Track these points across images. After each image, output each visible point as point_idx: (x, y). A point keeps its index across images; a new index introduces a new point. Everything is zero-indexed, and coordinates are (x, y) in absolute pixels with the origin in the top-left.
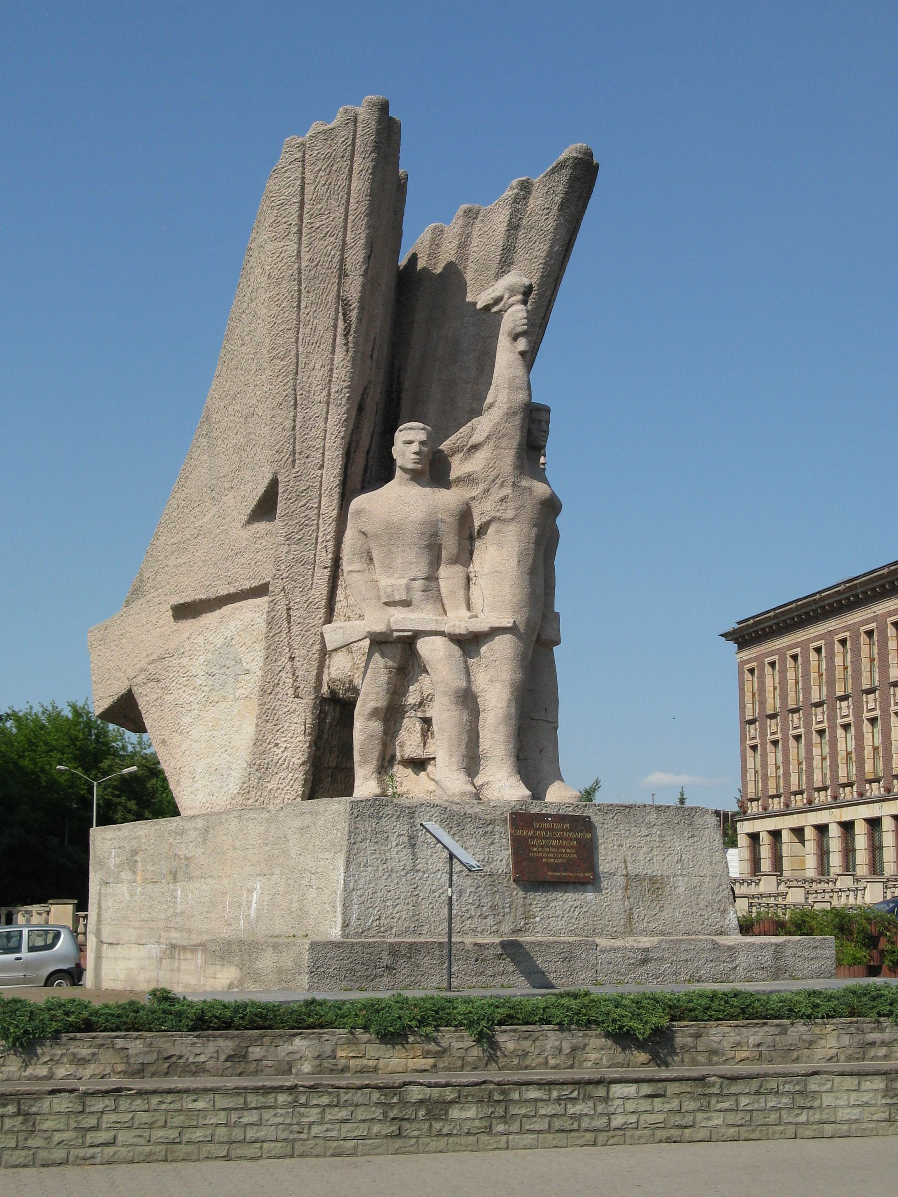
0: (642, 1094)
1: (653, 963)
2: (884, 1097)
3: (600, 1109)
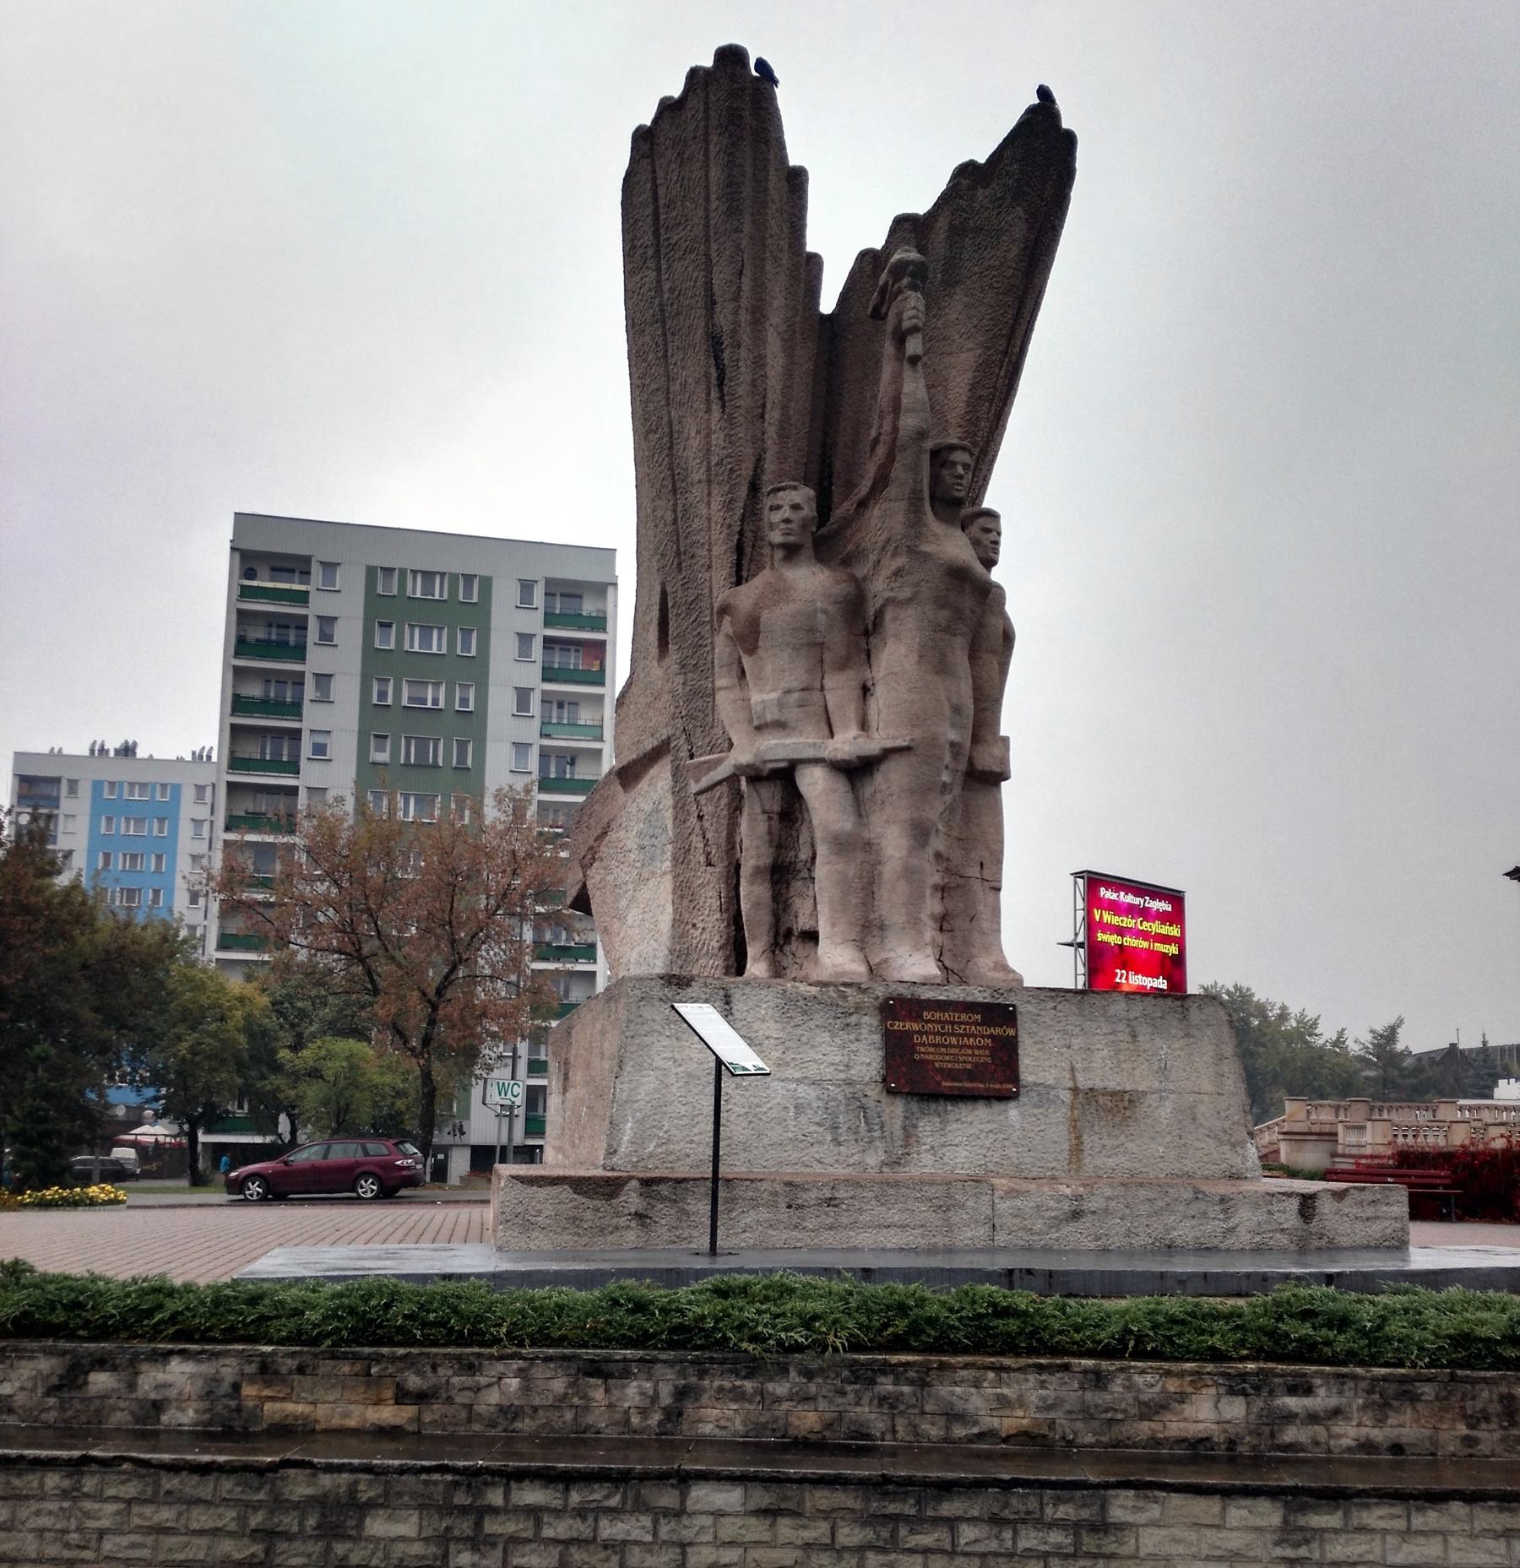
0: (752, 1506)
1: (1090, 1217)
2: (1277, 1544)
3: (665, 1530)
